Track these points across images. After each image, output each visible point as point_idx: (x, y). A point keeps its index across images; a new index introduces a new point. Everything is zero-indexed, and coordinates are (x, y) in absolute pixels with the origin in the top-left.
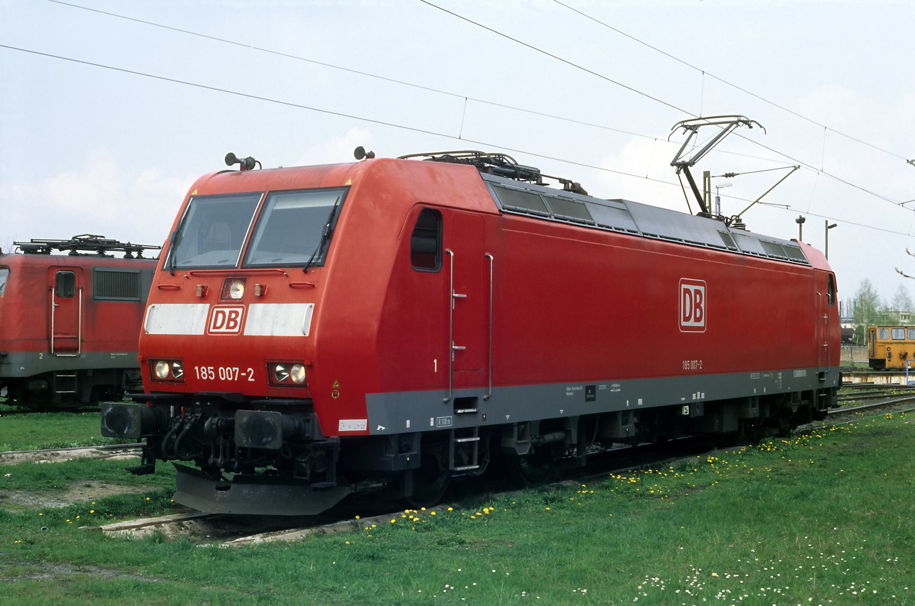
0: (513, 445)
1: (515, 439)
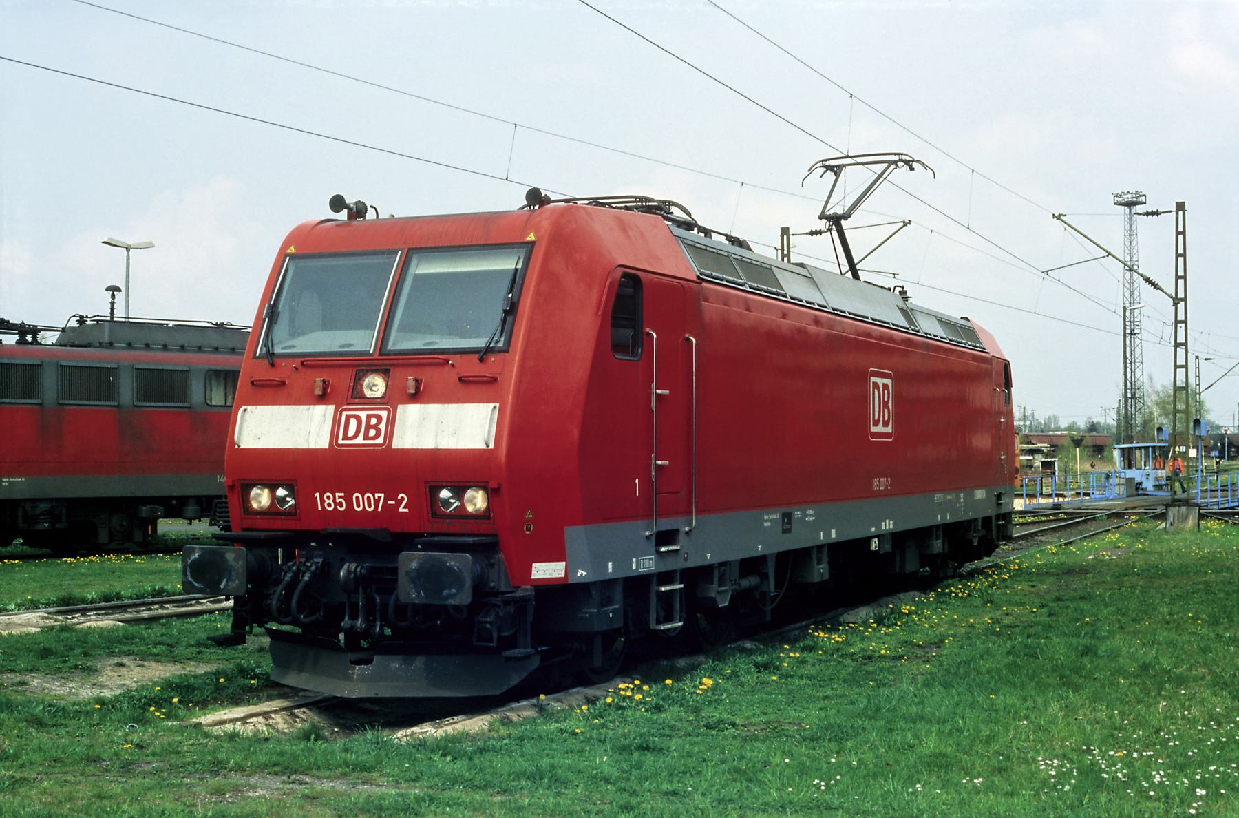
0: (713, 594)
1: (715, 586)
